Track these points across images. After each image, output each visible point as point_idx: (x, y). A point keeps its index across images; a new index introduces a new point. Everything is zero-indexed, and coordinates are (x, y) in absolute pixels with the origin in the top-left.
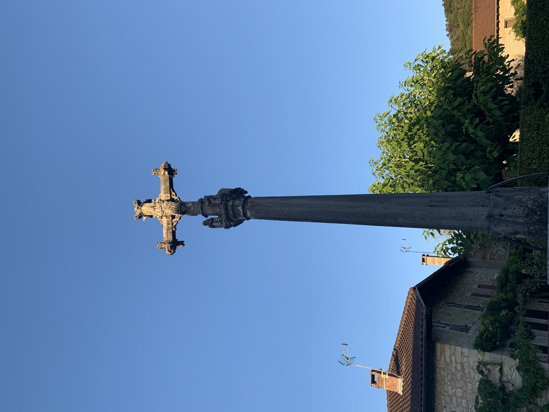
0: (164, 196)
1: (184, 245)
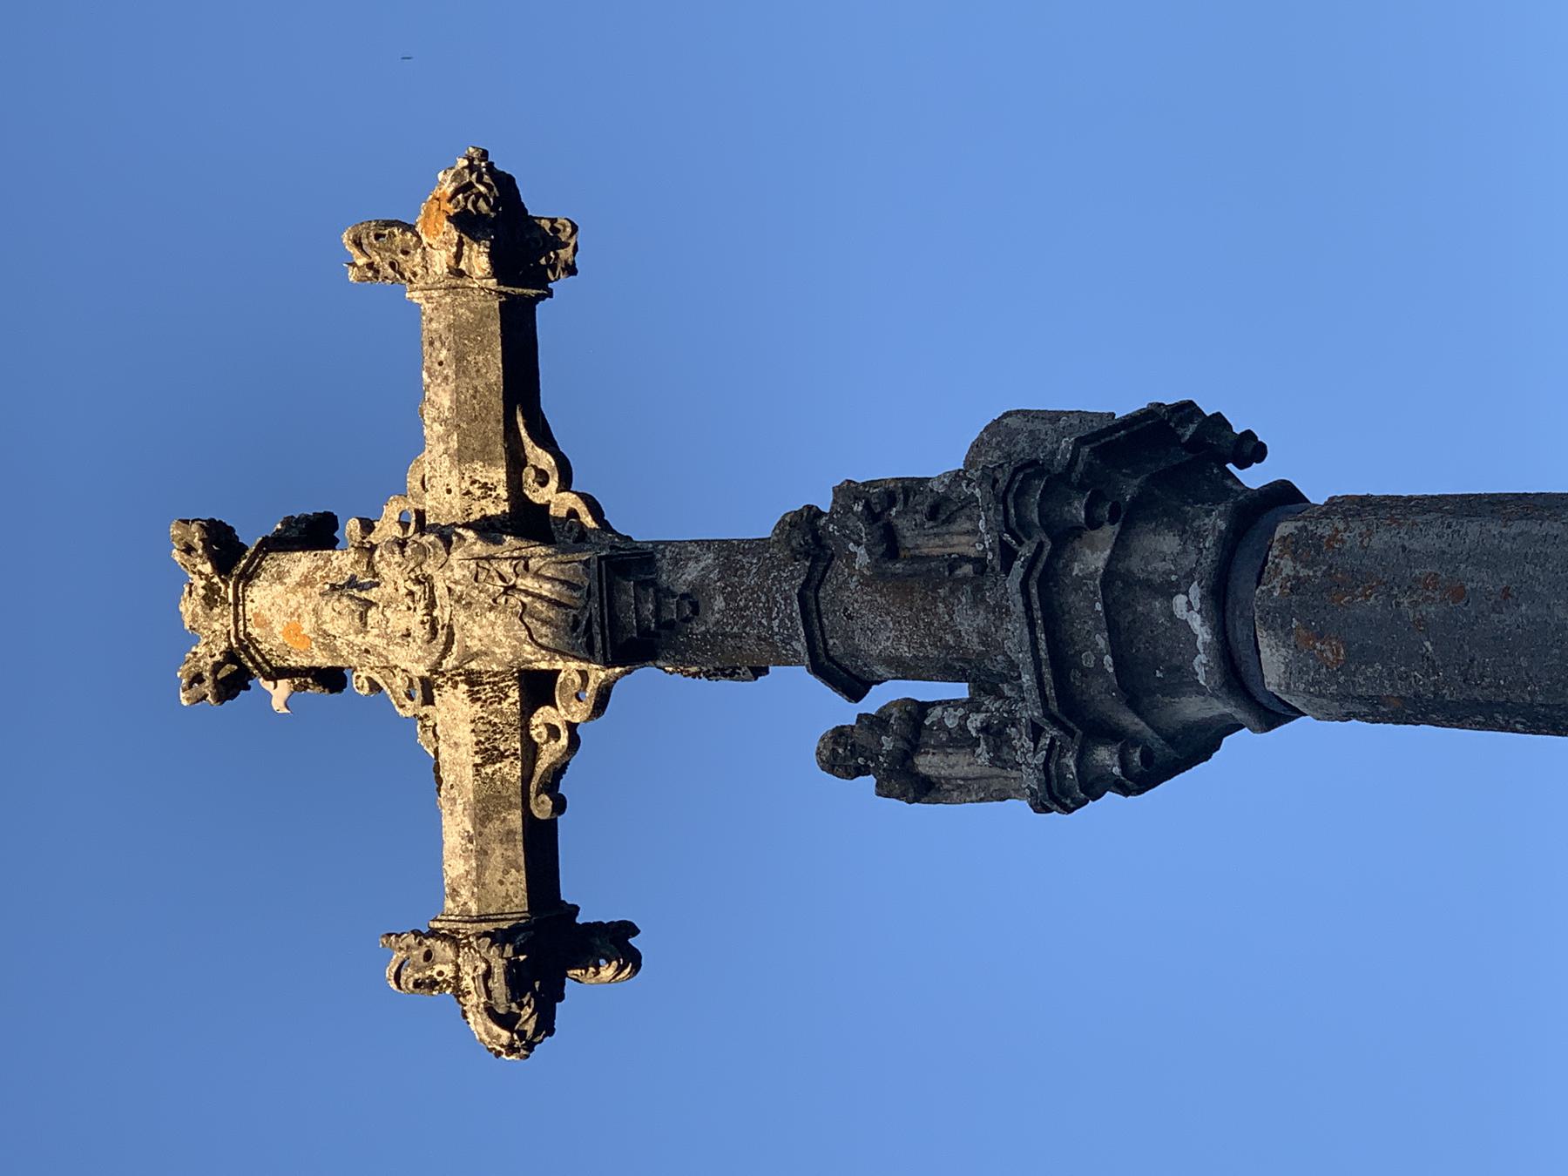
0: (453, 481)
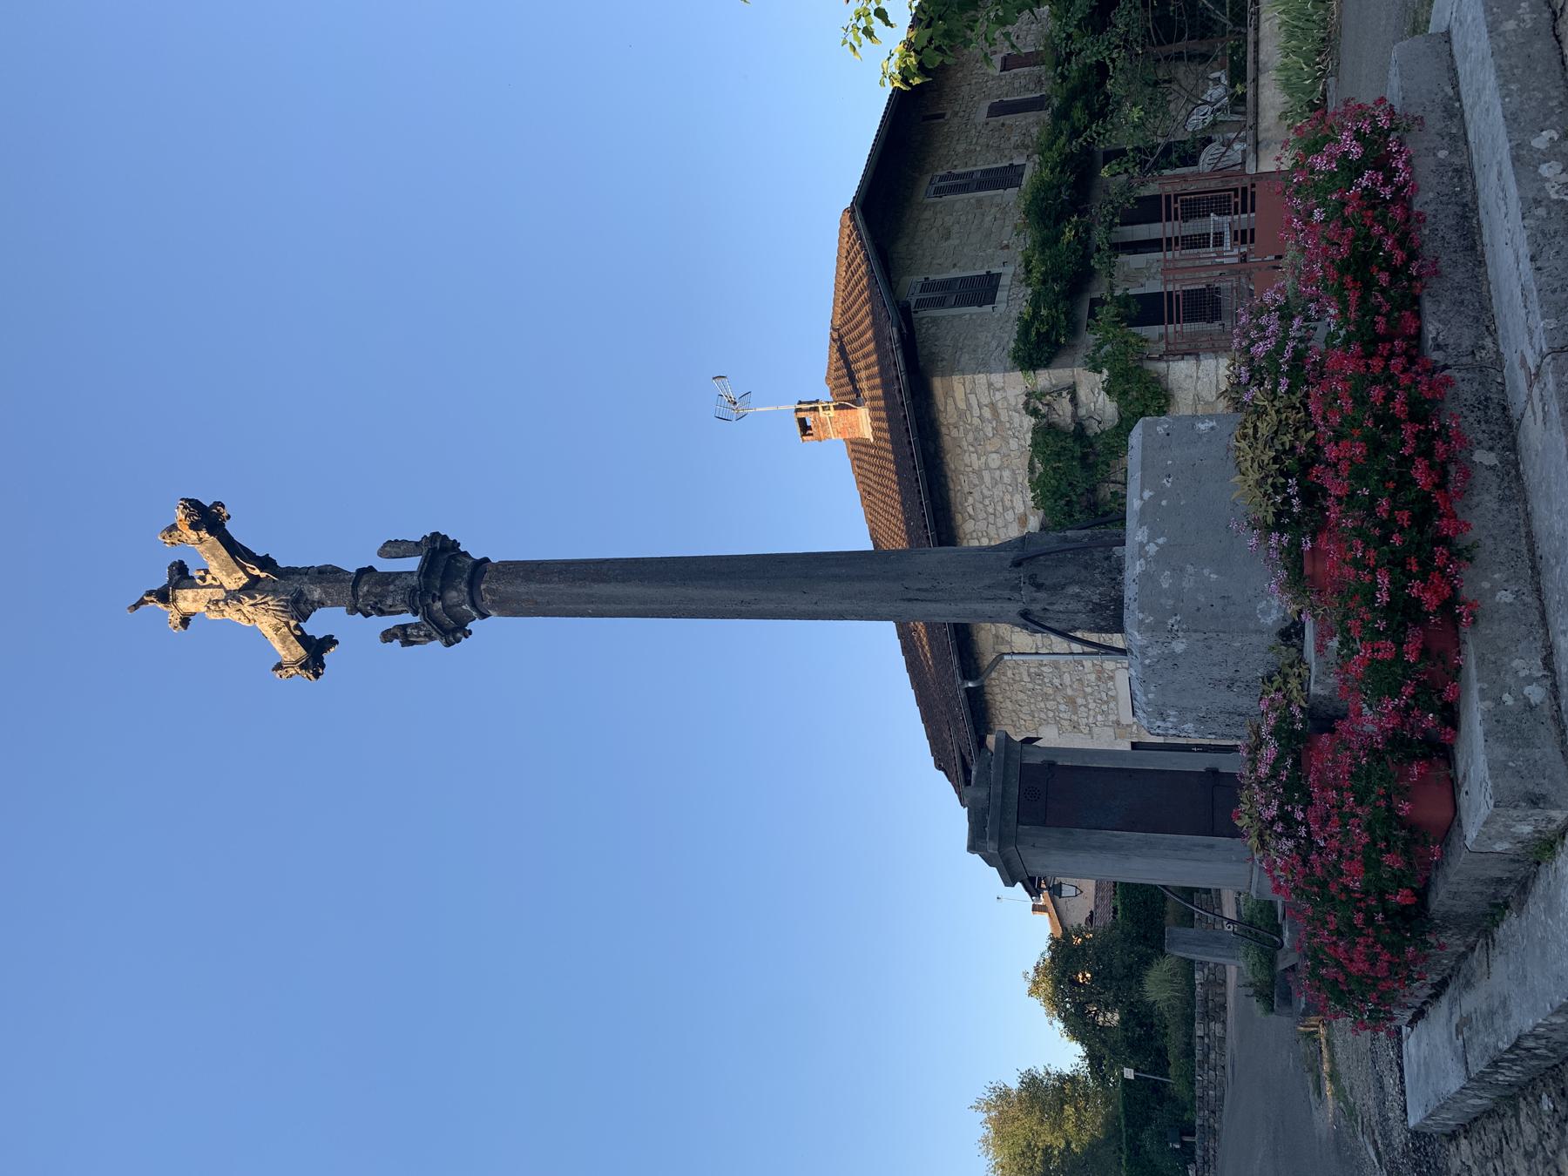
0: (230, 581)
1: (336, 642)
